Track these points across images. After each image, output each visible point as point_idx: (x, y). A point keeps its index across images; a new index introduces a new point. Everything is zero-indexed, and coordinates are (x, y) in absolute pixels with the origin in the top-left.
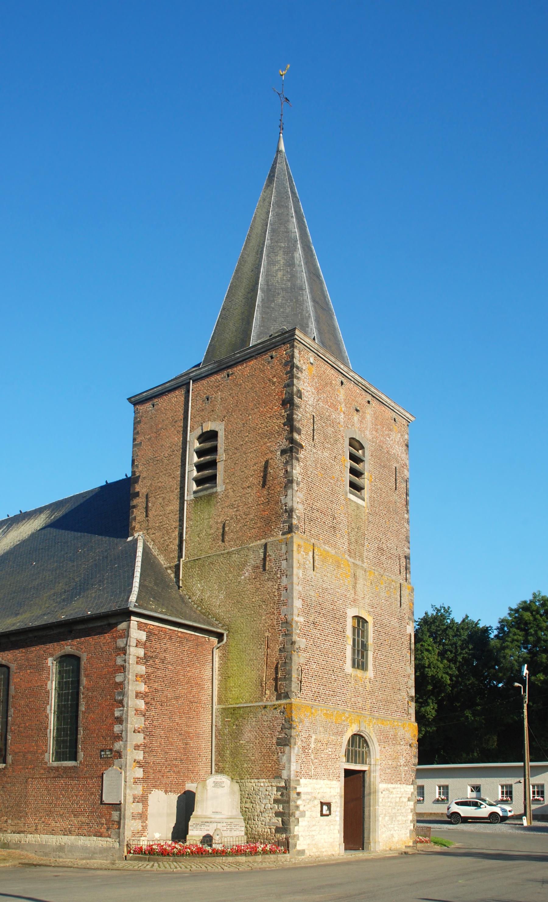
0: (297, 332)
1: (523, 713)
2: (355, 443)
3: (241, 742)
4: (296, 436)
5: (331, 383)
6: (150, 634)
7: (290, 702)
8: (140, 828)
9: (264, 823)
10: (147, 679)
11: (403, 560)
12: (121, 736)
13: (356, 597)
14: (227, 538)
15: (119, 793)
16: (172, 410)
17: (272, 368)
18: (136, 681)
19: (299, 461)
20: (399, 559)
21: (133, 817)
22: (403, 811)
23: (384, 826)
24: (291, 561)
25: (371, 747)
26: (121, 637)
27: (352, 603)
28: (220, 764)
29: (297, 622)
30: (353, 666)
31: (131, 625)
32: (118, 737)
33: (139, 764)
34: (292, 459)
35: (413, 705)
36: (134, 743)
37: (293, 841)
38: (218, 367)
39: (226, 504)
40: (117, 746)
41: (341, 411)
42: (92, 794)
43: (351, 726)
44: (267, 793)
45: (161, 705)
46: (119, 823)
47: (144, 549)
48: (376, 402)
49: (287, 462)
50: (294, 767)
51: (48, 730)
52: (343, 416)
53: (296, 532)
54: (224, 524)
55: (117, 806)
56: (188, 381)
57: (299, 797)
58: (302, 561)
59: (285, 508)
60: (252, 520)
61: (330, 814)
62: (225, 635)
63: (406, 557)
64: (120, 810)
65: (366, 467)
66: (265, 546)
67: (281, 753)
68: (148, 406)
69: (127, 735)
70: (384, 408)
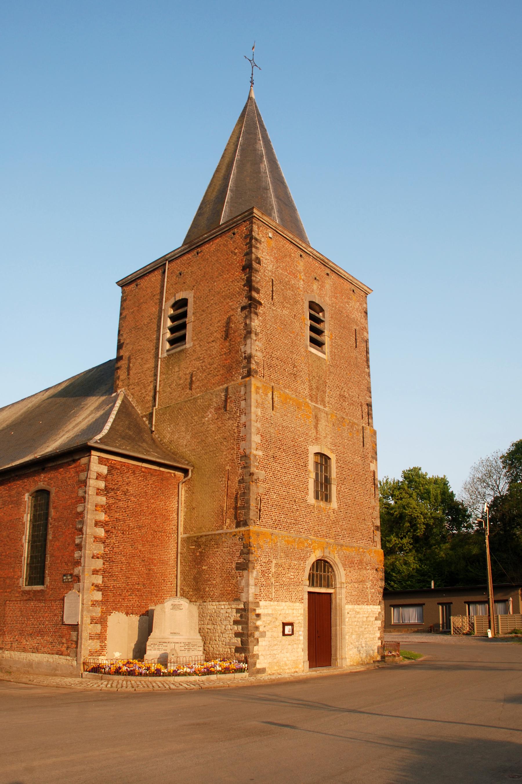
0: (255, 211)
1: (485, 543)
2: (313, 305)
3: (204, 568)
4: (255, 295)
5: (290, 256)
6: (111, 468)
7: (248, 529)
8: (98, 648)
9: (224, 643)
10: (107, 509)
11: (365, 407)
12: (80, 562)
13: (318, 436)
14: (194, 386)
15: (77, 614)
16: (151, 287)
17: (234, 242)
18: (96, 510)
19: (258, 315)
20: (361, 406)
21: (91, 638)
22: (371, 629)
23: (351, 643)
24: (249, 400)
25: (336, 572)
26: (83, 471)
27: (314, 441)
28: (184, 588)
29: (255, 456)
30: (317, 498)
31: (92, 459)
32: (78, 563)
33: (98, 588)
34: (251, 313)
35: (378, 533)
36: (92, 568)
37: (252, 660)
38: (189, 247)
39: (194, 358)
40: (77, 571)
41: (301, 279)
42: (55, 615)
43: (314, 552)
44: (227, 615)
45: (123, 533)
46: (77, 643)
47: (123, 401)
48: (334, 274)
49: (246, 317)
50: (252, 590)
51: (23, 558)
52: (302, 283)
53: (255, 375)
54: (192, 375)
55: (75, 627)
56: (165, 262)
57: (258, 618)
58: (260, 401)
59: (244, 355)
60: (216, 369)
61: (293, 634)
62: (190, 471)
63: (367, 405)
64: (78, 631)
65: (326, 326)
66: (227, 390)
67: (240, 577)
68: (133, 285)
69: (85, 560)
70: (342, 281)
